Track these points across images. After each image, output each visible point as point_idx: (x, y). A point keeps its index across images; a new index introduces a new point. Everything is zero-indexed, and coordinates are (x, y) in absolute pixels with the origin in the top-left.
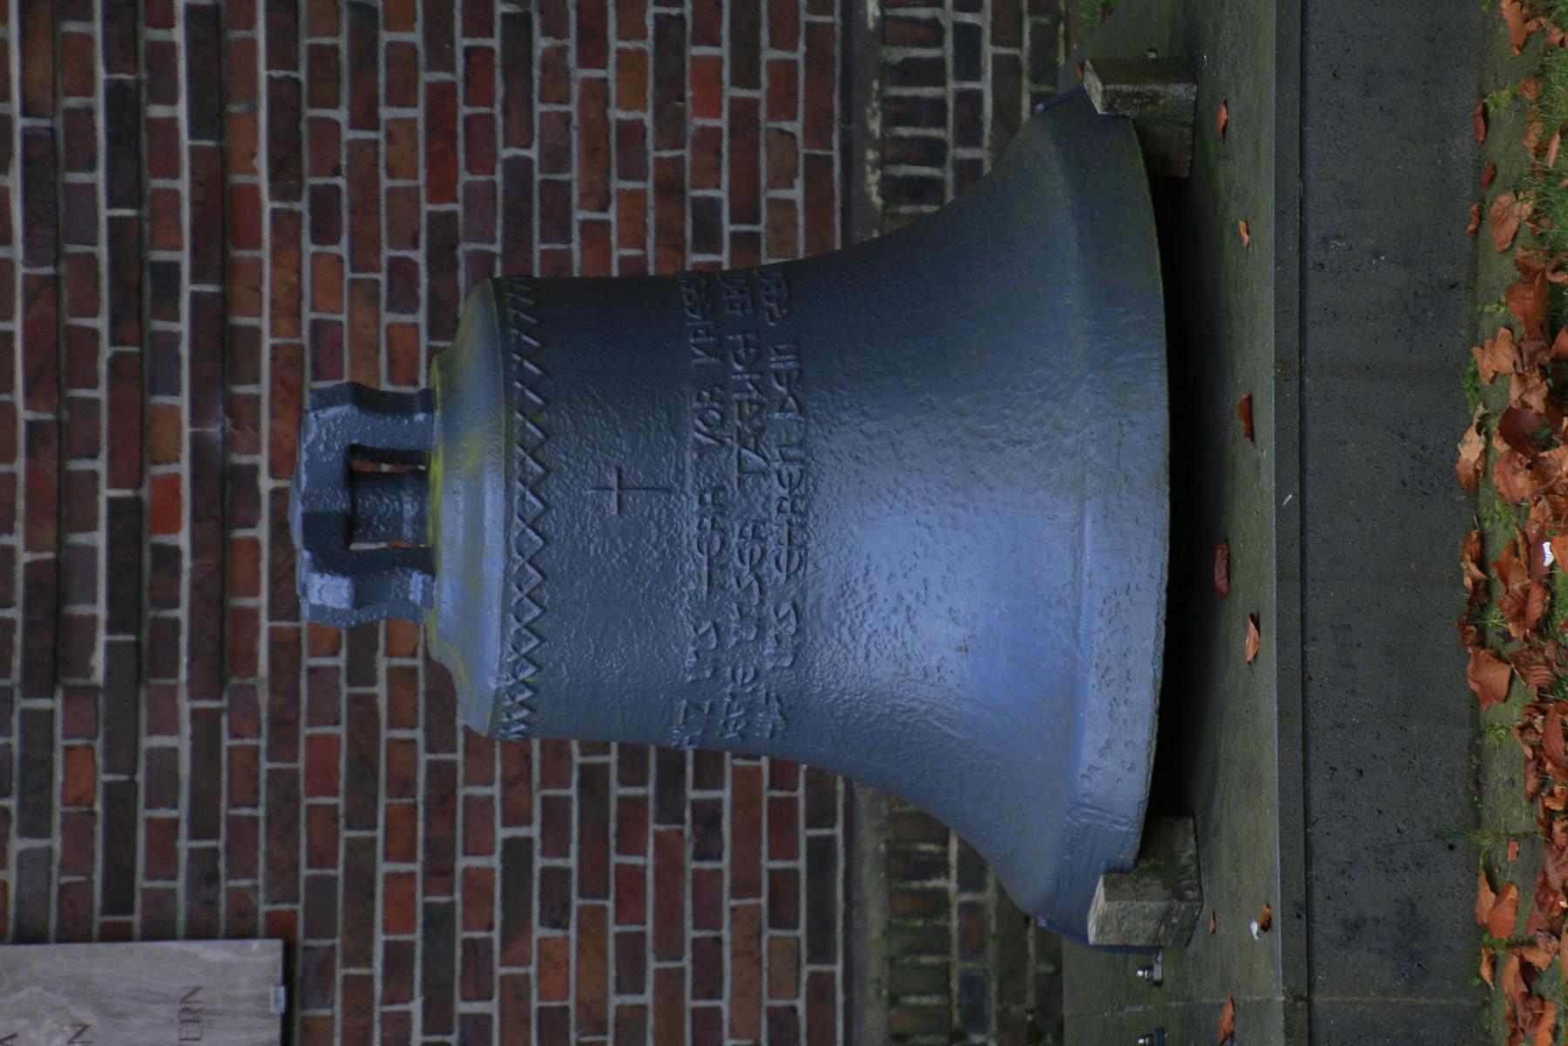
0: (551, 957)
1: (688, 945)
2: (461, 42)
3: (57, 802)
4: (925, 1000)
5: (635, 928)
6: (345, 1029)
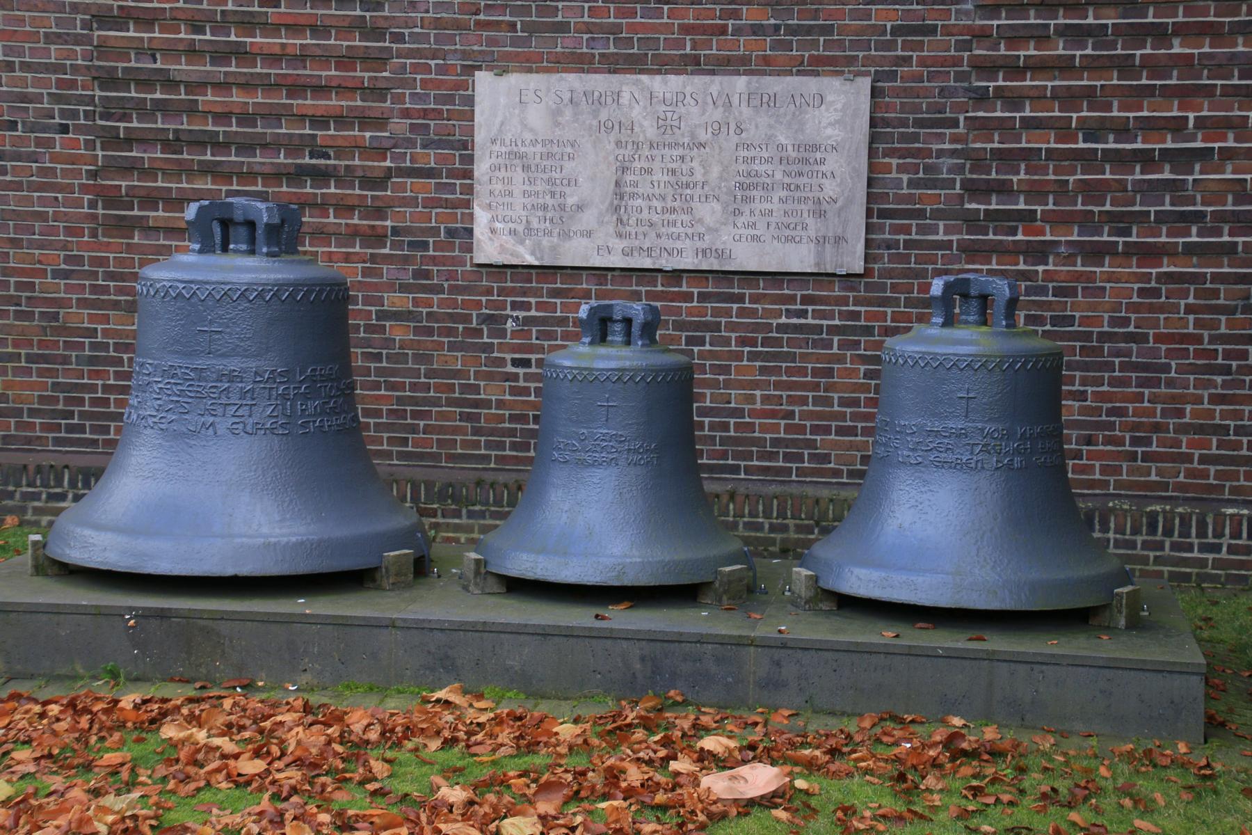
2: (1220, 348)
3: (920, 191)
4: (831, 512)
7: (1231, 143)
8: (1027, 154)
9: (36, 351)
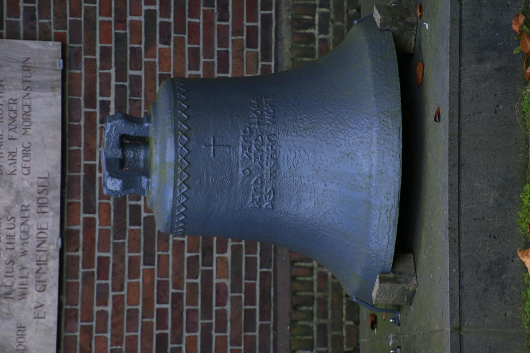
1: (216, 53)
5: (196, 46)
6: (86, 78)
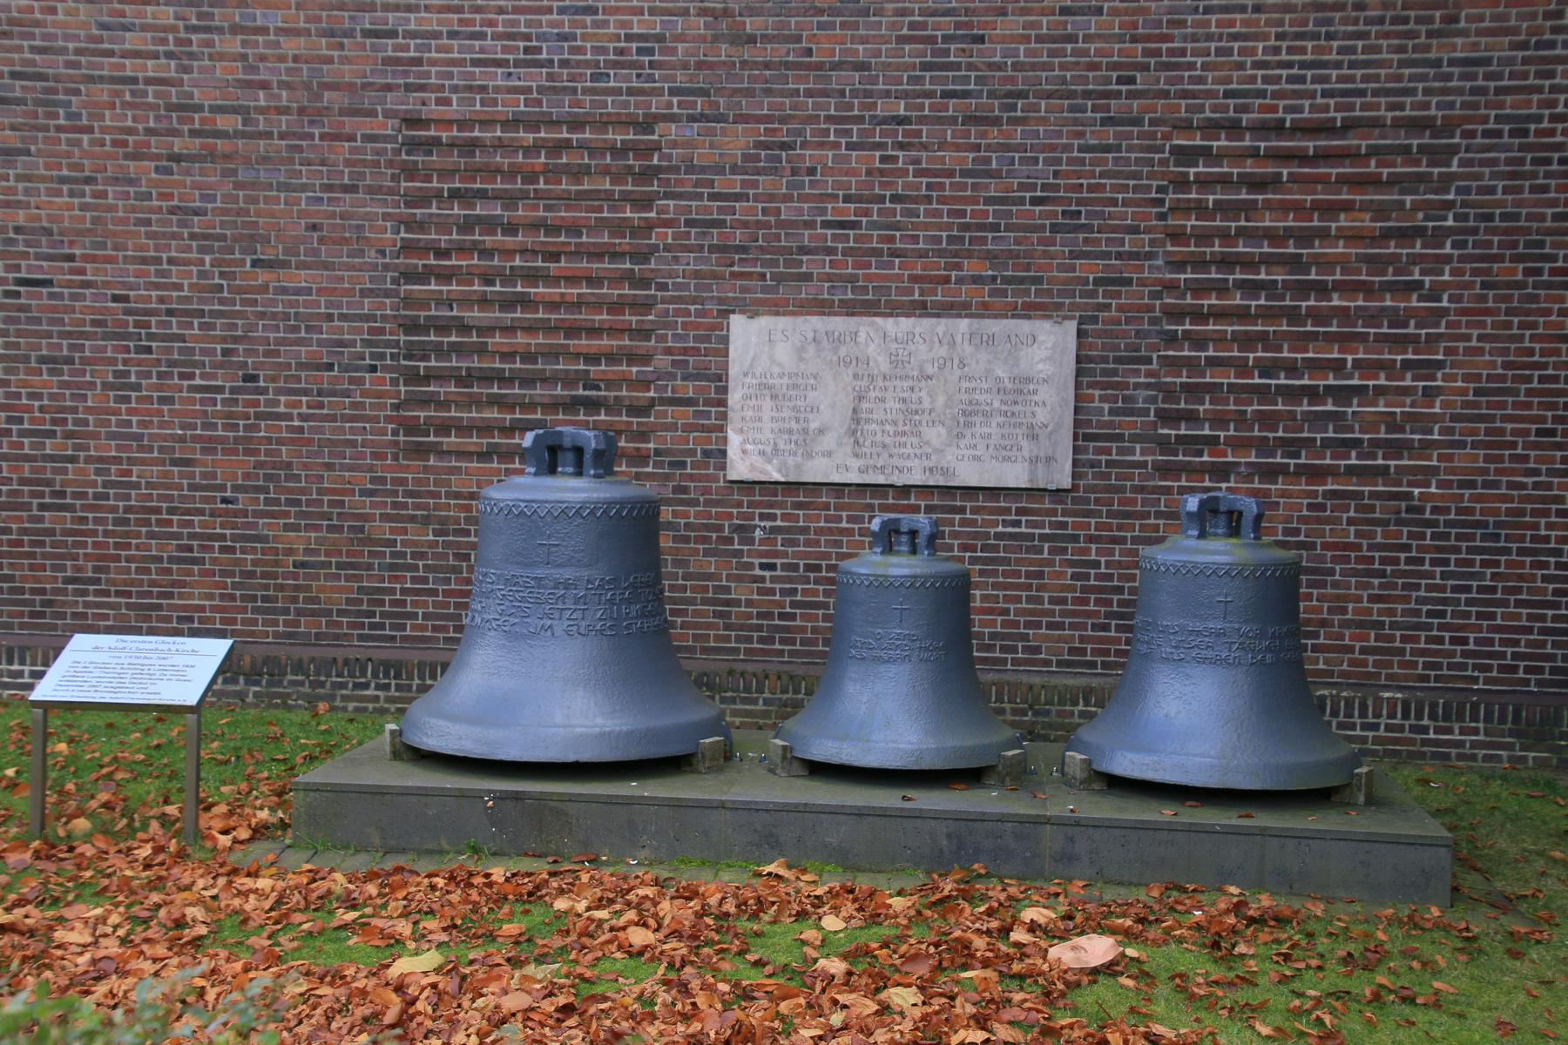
0: (1061, 575)
2: (1377, 555)
7: (1382, 382)
8: (1212, 388)
9: (344, 559)
